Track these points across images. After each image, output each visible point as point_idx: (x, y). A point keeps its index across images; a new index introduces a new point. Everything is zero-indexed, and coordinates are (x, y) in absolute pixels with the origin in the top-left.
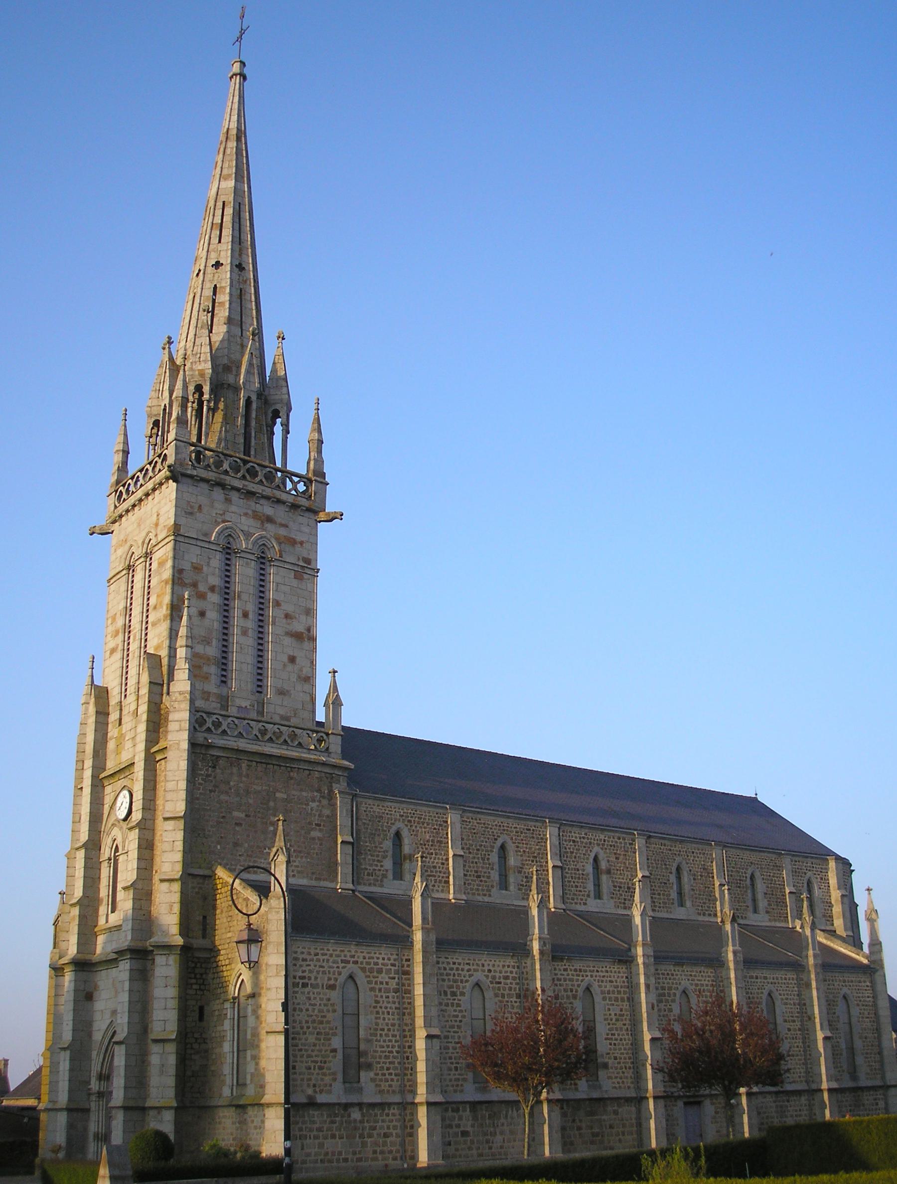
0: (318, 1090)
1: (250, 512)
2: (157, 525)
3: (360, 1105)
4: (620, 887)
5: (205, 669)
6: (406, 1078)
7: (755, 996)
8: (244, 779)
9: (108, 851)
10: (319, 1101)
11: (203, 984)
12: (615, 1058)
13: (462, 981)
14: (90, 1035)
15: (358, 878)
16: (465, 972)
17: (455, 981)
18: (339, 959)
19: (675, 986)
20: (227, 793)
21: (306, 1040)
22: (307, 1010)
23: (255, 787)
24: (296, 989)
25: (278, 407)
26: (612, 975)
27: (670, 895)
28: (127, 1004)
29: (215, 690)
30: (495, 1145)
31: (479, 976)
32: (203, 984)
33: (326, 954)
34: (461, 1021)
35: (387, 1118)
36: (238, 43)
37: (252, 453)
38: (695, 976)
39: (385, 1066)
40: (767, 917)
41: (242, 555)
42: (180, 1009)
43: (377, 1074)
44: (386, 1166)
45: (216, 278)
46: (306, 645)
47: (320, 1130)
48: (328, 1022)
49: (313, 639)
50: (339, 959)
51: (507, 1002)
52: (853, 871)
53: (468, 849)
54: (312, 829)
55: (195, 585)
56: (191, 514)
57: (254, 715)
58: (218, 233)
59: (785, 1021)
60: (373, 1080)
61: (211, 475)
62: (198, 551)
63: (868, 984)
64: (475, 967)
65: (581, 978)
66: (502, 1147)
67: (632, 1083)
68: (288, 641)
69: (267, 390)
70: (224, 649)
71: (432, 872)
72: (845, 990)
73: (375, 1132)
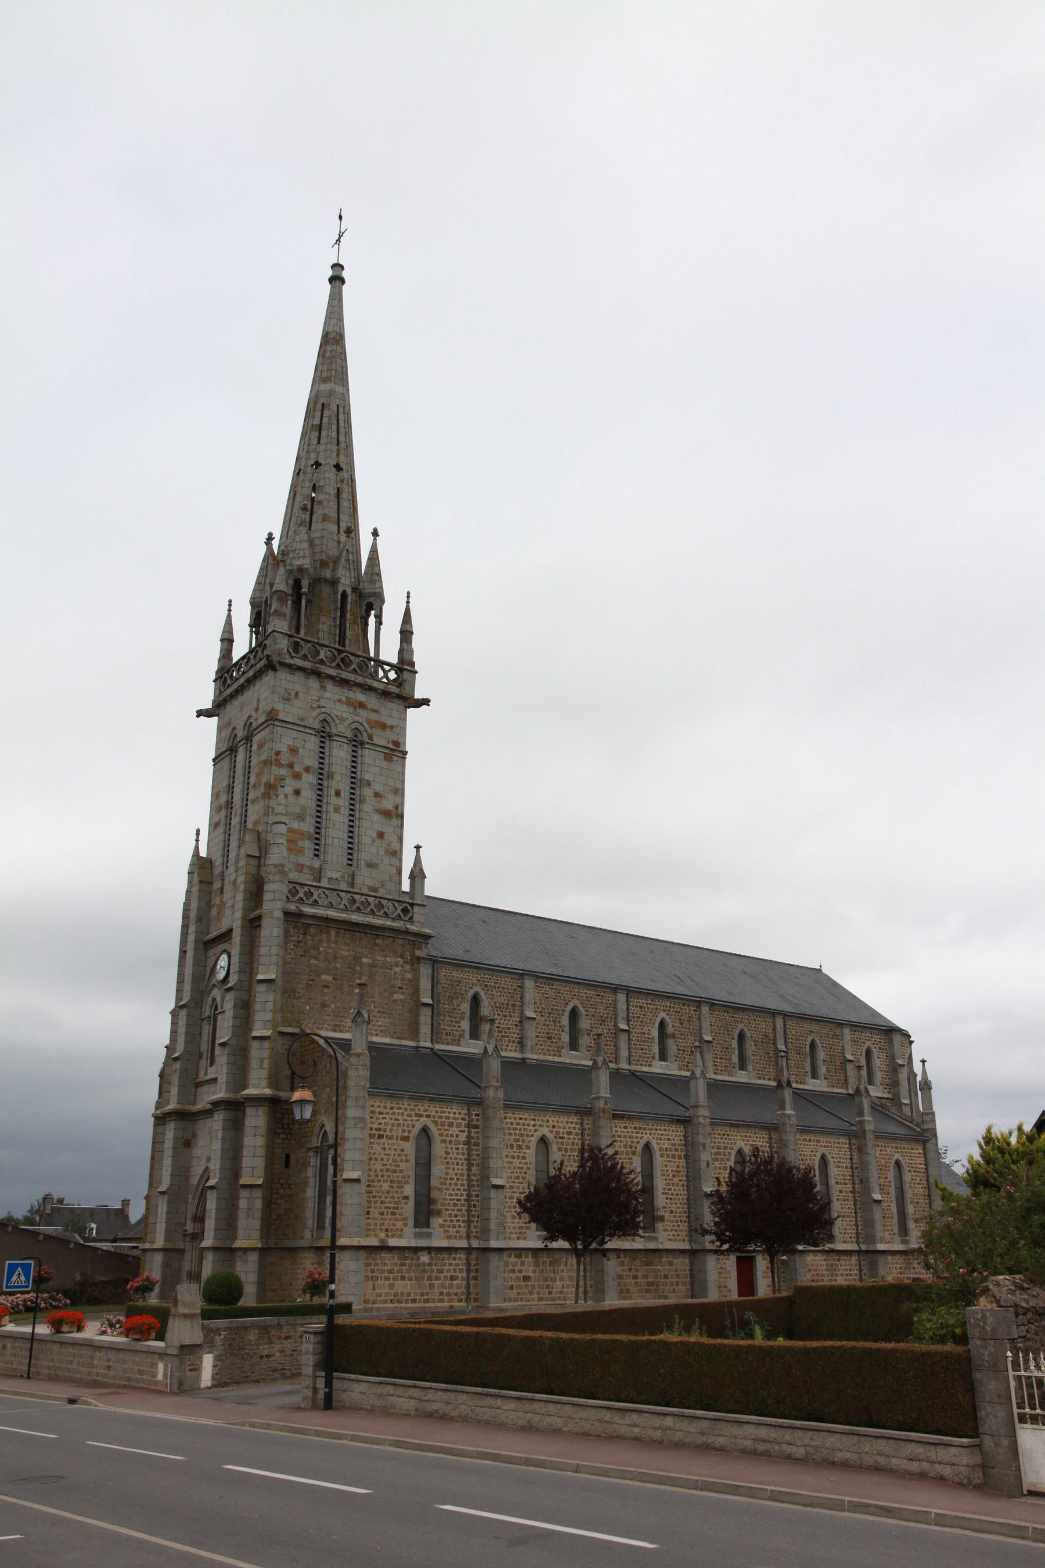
0: (390, 1234)
1: (343, 699)
2: (257, 709)
3: (429, 1249)
4: (684, 1051)
5: (300, 843)
6: (472, 1225)
7: (808, 1158)
8: (333, 945)
9: (208, 1009)
10: (390, 1245)
11: (290, 1134)
12: (671, 1212)
13: (527, 1136)
14: (187, 1179)
15: (437, 1038)
16: (531, 1128)
17: (521, 1135)
18: (413, 1113)
19: (729, 1146)
20: (316, 958)
21: (381, 1187)
22: (382, 1159)
23: (343, 952)
24: (372, 1140)
25: (372, 600)
26: (670, 1133)
27: (731, 1059)
28: (219, 1152)
29: (308, 863)
30: (554, 1290)
31: (545, 1131)
32: (290, 1134)
33: (401, 1108)
34: (525, 1173)
35: (454, 1262)
36: (337, 246)
37: (347, 643)
38: (750, 1137)
39: (454, 1213)
40: (825, 1082)
41: (336, 738)
42: (267, 1157)
43: (445, 1221)
44: (452, 1307)
45: (315, 478)
46: (395, 821)
47: (391, 1271)
48: (401, 1171)
49: (402, 817)
50: (413, 1113)
51: (570, 1156)
52: (913, 1042)
53: (541, 1012)
54: (395, 992)
55: (291, 766)
56: (288, 700)
57: (343, 886)
58: (317, 434)
59: (837, 1183)
60: (441, 1226)
61: (307, 664)
62: (294, 734)
63: (921, 1151)
64: (540, 1123)
65: (640, 1135)
66: (561, 1292)
67: (686, 1236)
68: (377, 818)
69: (362, 584)
70: (318, 825)
71: (506, 1032)
72: (897, 1156)
73: (442, 1275)
